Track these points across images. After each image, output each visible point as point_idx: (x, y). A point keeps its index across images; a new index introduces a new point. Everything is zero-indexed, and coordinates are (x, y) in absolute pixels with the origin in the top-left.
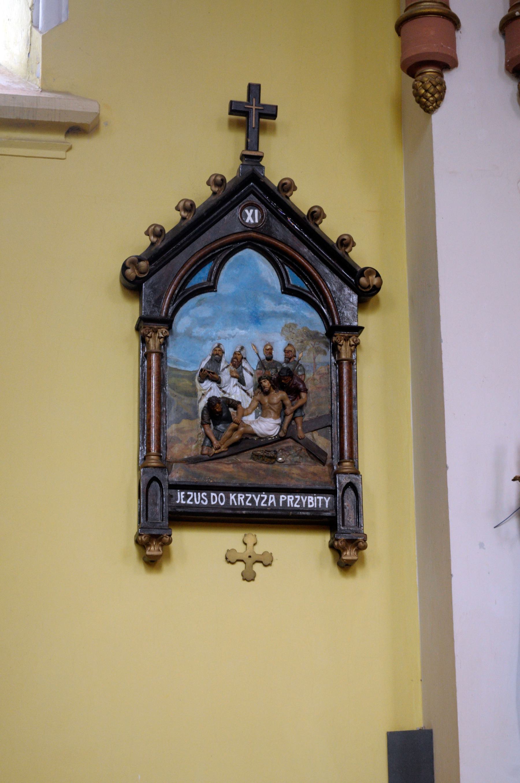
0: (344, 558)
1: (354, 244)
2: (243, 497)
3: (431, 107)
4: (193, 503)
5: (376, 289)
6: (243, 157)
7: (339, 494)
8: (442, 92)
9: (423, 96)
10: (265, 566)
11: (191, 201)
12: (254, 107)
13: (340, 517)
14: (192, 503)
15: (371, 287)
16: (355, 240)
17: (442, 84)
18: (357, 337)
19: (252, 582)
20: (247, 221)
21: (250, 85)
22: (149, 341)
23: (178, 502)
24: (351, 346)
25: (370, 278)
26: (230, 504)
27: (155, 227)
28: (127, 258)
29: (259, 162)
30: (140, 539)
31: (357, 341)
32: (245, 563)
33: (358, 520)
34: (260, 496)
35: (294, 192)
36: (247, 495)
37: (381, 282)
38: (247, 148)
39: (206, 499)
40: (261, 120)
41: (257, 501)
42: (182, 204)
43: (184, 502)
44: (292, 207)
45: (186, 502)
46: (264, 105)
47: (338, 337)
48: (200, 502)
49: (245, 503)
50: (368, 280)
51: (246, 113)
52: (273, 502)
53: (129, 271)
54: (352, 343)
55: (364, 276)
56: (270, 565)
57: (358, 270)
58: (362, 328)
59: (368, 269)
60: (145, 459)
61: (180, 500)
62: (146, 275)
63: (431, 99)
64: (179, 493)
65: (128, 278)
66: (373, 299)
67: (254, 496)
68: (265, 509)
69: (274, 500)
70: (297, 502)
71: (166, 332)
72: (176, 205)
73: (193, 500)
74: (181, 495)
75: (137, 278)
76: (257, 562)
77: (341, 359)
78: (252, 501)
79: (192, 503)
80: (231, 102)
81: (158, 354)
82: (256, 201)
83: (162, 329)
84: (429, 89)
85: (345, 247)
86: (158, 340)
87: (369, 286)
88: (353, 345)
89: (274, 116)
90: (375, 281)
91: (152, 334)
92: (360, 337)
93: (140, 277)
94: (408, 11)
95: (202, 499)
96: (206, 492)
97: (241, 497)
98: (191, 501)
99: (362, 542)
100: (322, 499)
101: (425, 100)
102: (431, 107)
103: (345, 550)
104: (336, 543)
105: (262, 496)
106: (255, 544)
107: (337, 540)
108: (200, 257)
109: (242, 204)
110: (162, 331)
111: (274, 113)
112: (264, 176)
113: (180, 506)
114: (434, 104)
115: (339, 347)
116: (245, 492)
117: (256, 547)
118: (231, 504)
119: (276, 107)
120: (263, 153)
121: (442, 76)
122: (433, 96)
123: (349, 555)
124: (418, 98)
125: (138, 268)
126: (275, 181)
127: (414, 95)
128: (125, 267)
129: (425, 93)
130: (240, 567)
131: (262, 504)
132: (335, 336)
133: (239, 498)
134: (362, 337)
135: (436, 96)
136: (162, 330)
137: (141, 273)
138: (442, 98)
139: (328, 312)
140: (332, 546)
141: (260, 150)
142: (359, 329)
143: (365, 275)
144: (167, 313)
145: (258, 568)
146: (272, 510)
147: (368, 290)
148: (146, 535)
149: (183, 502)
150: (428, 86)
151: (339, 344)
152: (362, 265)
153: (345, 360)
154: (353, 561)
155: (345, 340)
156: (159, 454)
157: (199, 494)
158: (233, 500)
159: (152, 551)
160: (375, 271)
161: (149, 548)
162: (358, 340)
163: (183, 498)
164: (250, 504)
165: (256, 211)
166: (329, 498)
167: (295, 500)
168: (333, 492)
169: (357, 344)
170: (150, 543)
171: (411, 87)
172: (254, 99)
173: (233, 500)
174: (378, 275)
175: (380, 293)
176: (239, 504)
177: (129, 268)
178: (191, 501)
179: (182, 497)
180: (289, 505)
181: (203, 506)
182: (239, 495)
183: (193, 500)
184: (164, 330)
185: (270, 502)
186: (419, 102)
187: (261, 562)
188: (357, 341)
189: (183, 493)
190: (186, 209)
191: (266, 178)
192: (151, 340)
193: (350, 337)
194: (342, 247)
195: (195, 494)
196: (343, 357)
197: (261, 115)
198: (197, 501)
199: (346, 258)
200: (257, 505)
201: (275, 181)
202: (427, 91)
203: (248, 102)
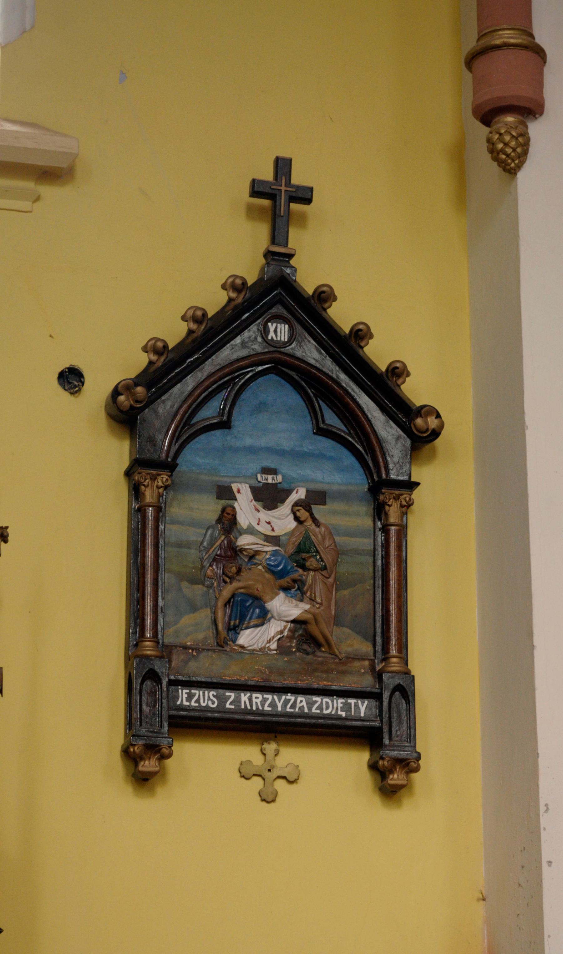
0: (141, 768)
1: (408, 375)
2: (261, 698)
3: (513, 165)
4: (199, 705)
5: (435, 434)
6: (268, 254)
7: (386, 696)
8: (526, 146)
9: (502, 151)
10: (291, 782)
11: (203, 309)
12: (283, 188)
13: (385, 729)
14: (197, 705)
15: (429, 433)
16: (409, 369)
17: (525, 135)
18: (410, 495)
19: (272, 805)
20: (270, 338)
21: (277, 160)
22: (145, 491)
23: (179, 703)
24: (402, 506)
25: (429, 419)
26: (241, 706)
27: (156, 342)
28: (119, 381)
29: (288, 262)
30: (132, 750)
31: (410, 499)
32: (264, 779)
33: (408, 731)
34: (286, 697)
35: (334, 303)
36: (265, 696)
37: (442, 426)
38: (273, 241)
39: (215, 700)
40: (293, 206)
41: (279, 705)
42: (191, 313)
43: (188, 704)
44: (369, 362)
45: (190, 704)
46: (298, 187)
47: (386, 494)
48: (208, 704)
49: (263, 706)
50: (426, 422)
51: (272, 196)
52: (303, 706)
53: (122, 398)
54: (160, 484)
55: (421, 416)
56: (273, 801)
57: (414, 408)
58: (418, 484)
59: (427, 408)
60: (136, 645)
61: (182, 701)
62: (142, 405)
63: (513, 154)
64: (180, 691)
65: (122, 408)
66: (428, 447)
67: (275, 697)
68: (290, 715)
69: (304, 703)
70: (196, 698)
71: (167, 480)
72: (182, 314)
73: (198, 701)
74: (183, 693)
75: (132, 407)
76: (279, 777)
77: (388, 523)
78: (273, 704)
79: (197, 705)
80: (254, 181)
81: (156, 508)
82: (285, 313)
83: (162, 476)
84: (508, 142)
85: (397, 378)
86: (157, 490)
87: (427, 430)
88: (405, 506)
89: (308, 201)
90: (432, 422)
91: (148, 483)
92: (413, 496)
93: (135, 406)
94: (480, 43)
95: (209, 699)
96: (215, 692)
97: (257, 698)
98: (196, 702)
99: (167, 748)
100: (355, 703)
101: (504, 157)
102: (513, 165)
103: (391, 772)
104: (381, 763)
105: (288, 697)
106: (276, 755)
107: (382, 758)
108: (212, 381)
109: (267, 316)
110: (163, 478)
111: (310, 197)
112: (295, 281)
113: (181, 708)
114: (517, 162)
115: (387, 508)
116: (264, 693)
117: (278, 758)
118: (243, 707)
119: (311, 189)
120: (295, 251)
121: (526, 127)
122: (514, 150)
123: (396, 778)
124: (495, 154)
125: (133, 394)
126: (309, 288)
127: (488, 151)
128: (116, 393)
129: (504, 147)
130: (257, 783)
131: (288, 710)
132: (383, 494)
133: (254, 700)
134: (416, 494)
135: (519, 150)
136: (163, 478)
137: (137, 401)
138: (525, 153)
139: (374, 465)
140: (373, 767)
141: (290, 245)
142: (411, 485)
143: (423, 416)
144: (167, 456)
145: (280, 785)
146: (300, 716)
147: (425, 435)
148: (140, 746)
149: (185, 703)
150: (507, 138)
151: (388, 503)
152: (418, 403)
153: (150, 506)
154: (402, 787)
155: (394, 498)
156: (155, 640)
157: (206, 692)
158: (245, 702)
159: (395, 780)
160: (435, 410)
161: (142, 763)
162: (412, 500)
163: (341, 707)
164: (270, 709)
165: (287, 326)
166: (366, 702)
167: (264, 700)
168: (376, 696)
169: (409, 505)
170: (144, 756)
171: (485, 142)
172: (284, 178)
173: (245, 702)
174: (438, 416)
175: (438, 442)
176: (254, 708)
177: (122, 395)
178: (196, 702)
179: (185, 696)
180: (243, 707)
181: (210, 710)
182: (254, 695)
183: (198, 701)
184: (165, 477)
185: (298, 705)
186: (496, 159)
187: (284, 778)
188: (410, 499)
189: (185, 691)
190: (195, 320)
191: (297, 282)
192: (147, 489)
193: (402, 495)
194: (393, 378)
195: (201, 693)
196: (392, 520)
197: (293, 199)
198: (204, 702)
199: (397, 391)
200: (280, 709)
201: (309, 288)
202: (506, 144)
203: (275, 181)
